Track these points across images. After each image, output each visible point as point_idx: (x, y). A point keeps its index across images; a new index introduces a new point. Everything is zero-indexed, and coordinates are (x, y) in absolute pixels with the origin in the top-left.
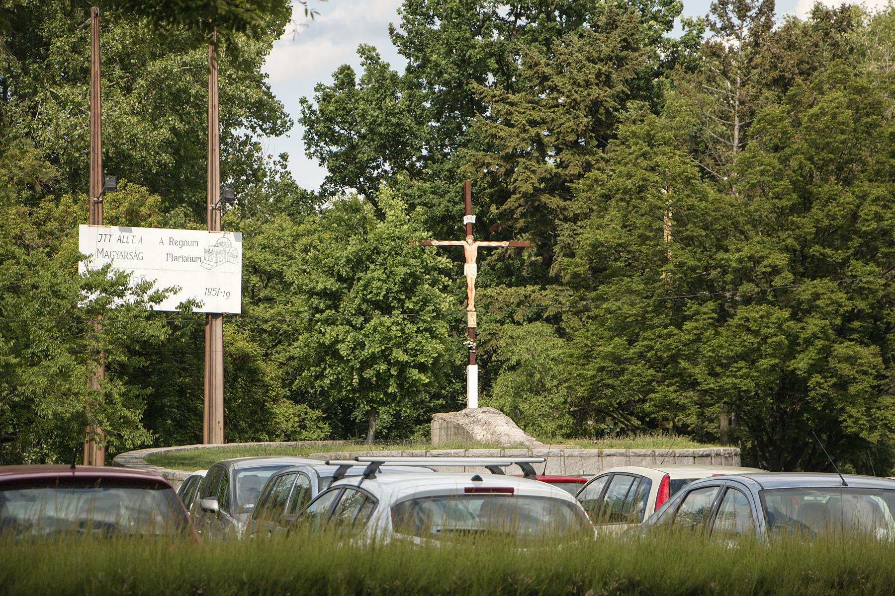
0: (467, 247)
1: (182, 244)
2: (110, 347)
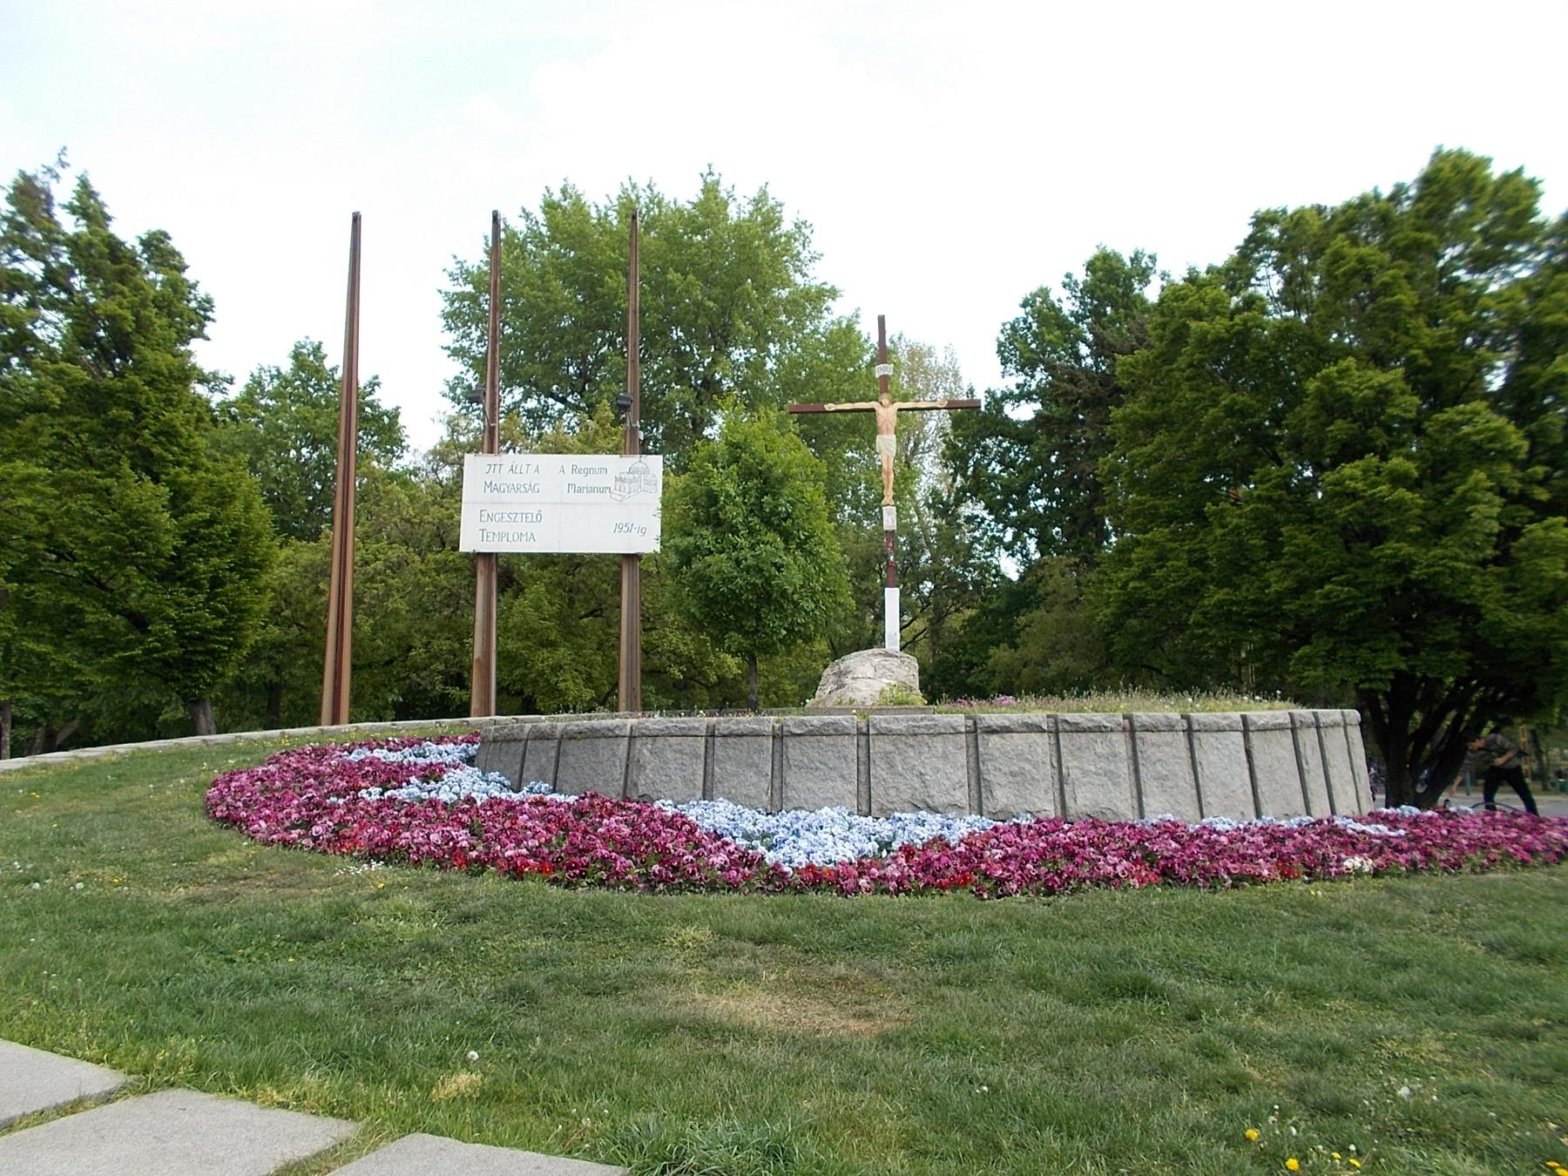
0: (880, 410)
1: (587, 472)
2: (1304, 941)
